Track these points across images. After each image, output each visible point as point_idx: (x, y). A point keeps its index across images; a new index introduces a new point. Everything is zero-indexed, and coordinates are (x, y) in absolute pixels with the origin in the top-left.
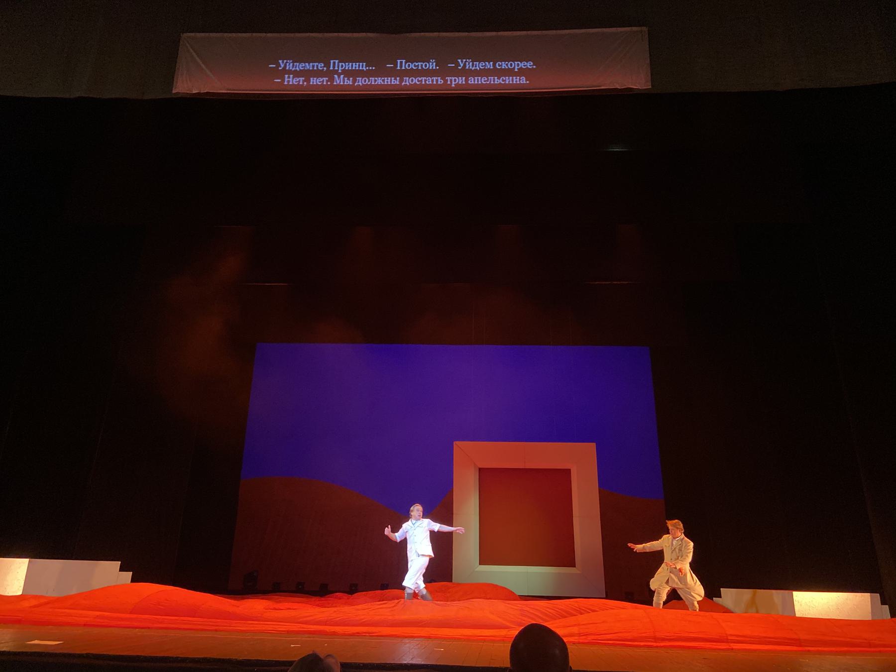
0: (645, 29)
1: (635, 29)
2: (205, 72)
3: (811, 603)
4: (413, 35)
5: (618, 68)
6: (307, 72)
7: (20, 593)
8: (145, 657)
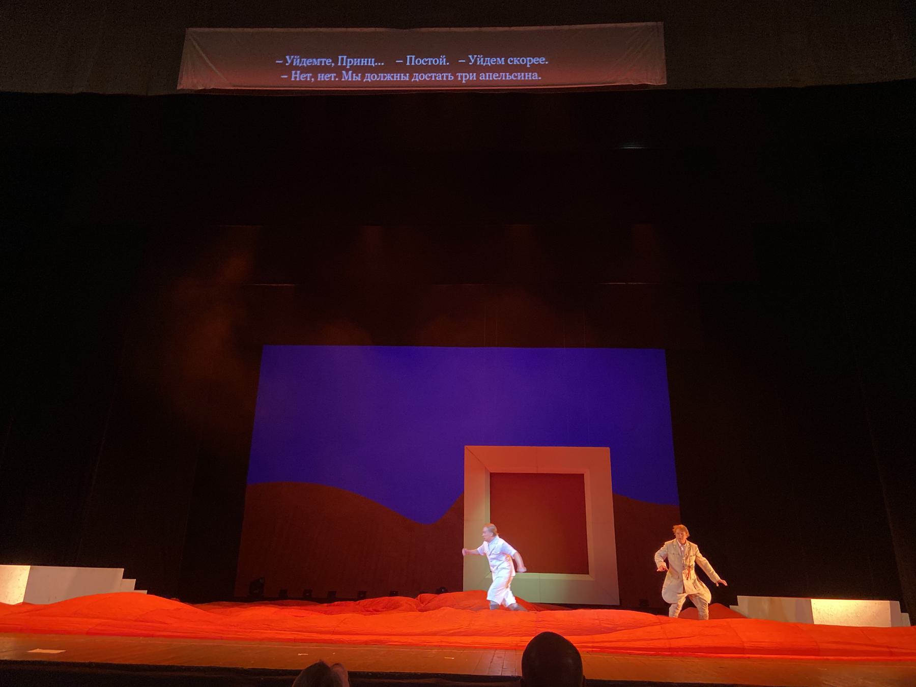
0: (660, 24)
1: (650, 24)
2: (207, 71)
3: (829, 611)
4: (424, 30)
5: (633, 63)
6: (313, 68)
7: (21, 601)
8: (149, 666)
